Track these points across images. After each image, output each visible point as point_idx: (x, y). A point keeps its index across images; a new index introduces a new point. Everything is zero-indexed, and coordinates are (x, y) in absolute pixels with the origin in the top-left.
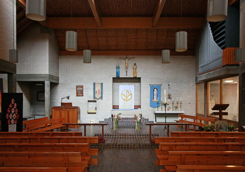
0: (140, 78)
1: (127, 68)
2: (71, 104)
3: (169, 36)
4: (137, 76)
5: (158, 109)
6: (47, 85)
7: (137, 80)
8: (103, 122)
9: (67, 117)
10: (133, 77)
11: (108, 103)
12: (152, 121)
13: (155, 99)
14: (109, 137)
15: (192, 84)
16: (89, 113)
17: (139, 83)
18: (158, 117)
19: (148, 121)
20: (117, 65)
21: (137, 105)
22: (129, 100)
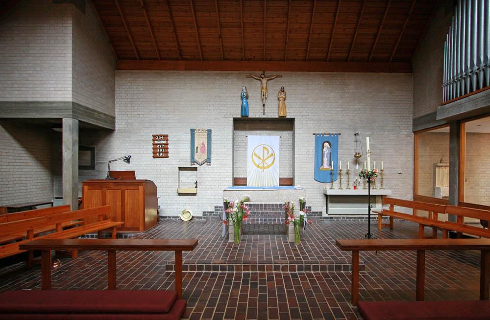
0: (292, 121)
1: (264, 98)
2: (132, 173)
3: (361, 24)
4: (288, 114)
5: (332, 185)
6: (68, 128)
7: (285, 124)
8: (213, 212)
9: (119, 204)
10: (277, 117)
11: (222, 174)
12: (319, 211)
13: (326, 165)
14: (204, 272)
15: (406, 133)
16: (180, 194)
17: (290, 132)
18: (332, 202)
19: (311, 210)
20: (243, 90)
21: (285, 177)
22: (269, 166)
